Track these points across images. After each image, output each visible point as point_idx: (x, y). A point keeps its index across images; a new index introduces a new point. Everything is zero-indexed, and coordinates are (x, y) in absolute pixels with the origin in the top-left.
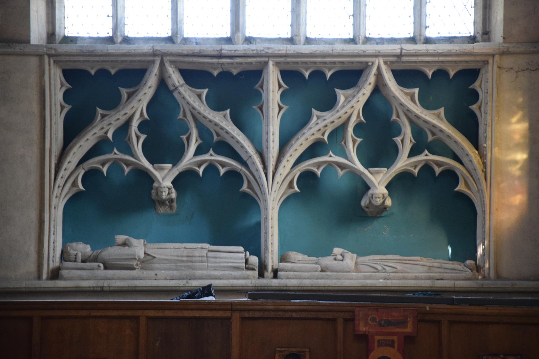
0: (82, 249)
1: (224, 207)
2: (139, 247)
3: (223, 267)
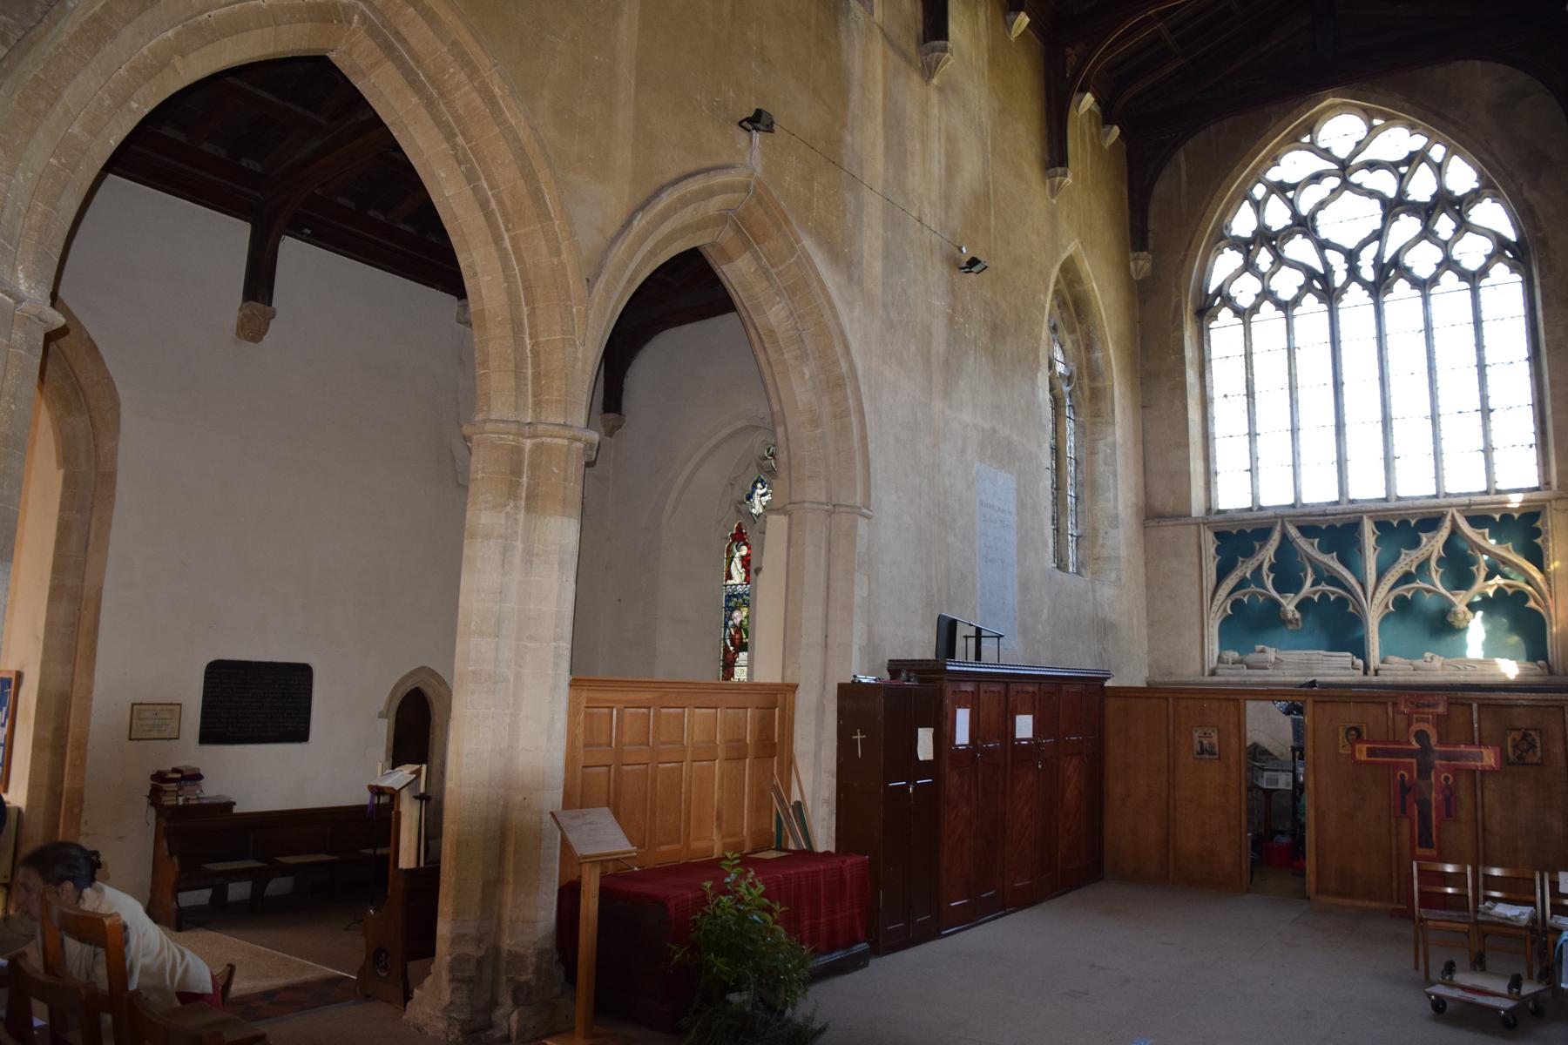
0: (1232, 655)
1: (1339, 625)
2: (1271, 654)
3: (1336, 667)
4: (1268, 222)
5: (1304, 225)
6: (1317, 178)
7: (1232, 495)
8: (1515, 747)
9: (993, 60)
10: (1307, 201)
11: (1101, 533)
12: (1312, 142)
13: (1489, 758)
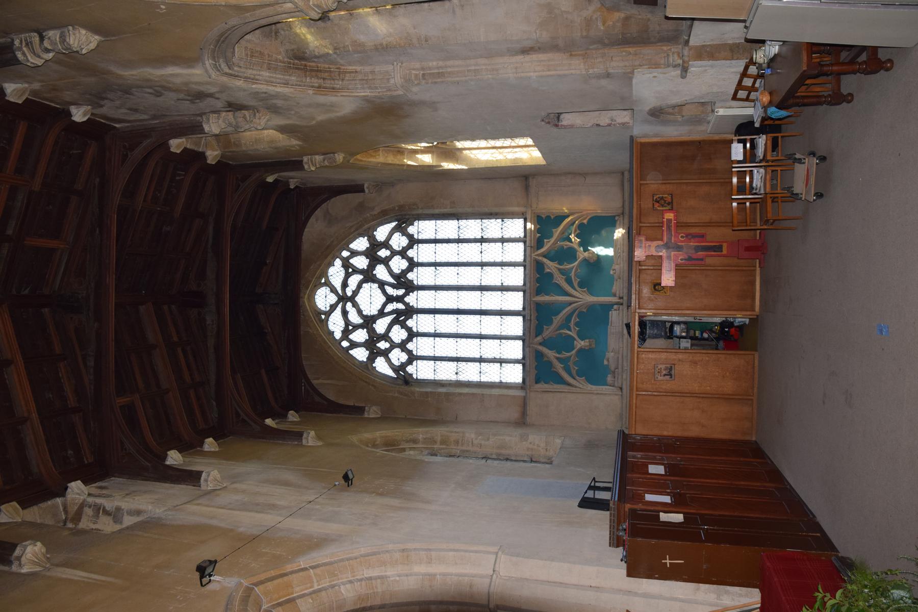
0: (610, 378)
2: (610, 355)
4: (363, 340)
5: (368, 322)
6: (345, 313)
7: (514, 374)
8: (663, 206)
9: (227, 459)
10: (354, 318)
11: (531, 446)
12: (325, 313)
13: (670, 216)
